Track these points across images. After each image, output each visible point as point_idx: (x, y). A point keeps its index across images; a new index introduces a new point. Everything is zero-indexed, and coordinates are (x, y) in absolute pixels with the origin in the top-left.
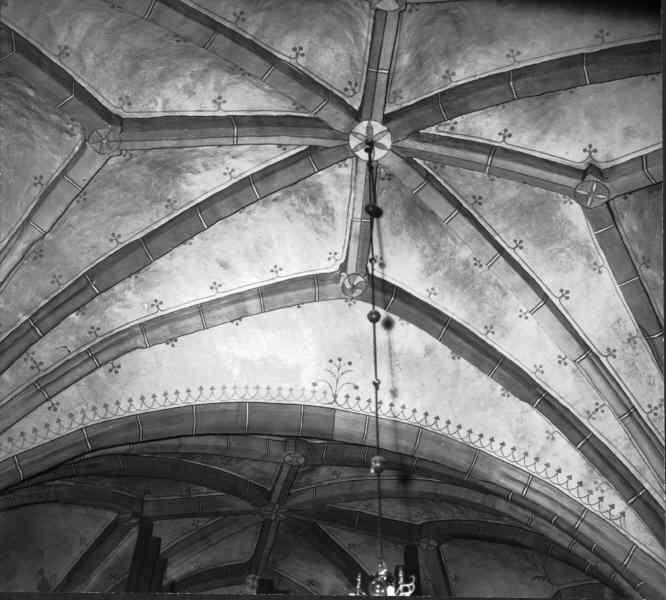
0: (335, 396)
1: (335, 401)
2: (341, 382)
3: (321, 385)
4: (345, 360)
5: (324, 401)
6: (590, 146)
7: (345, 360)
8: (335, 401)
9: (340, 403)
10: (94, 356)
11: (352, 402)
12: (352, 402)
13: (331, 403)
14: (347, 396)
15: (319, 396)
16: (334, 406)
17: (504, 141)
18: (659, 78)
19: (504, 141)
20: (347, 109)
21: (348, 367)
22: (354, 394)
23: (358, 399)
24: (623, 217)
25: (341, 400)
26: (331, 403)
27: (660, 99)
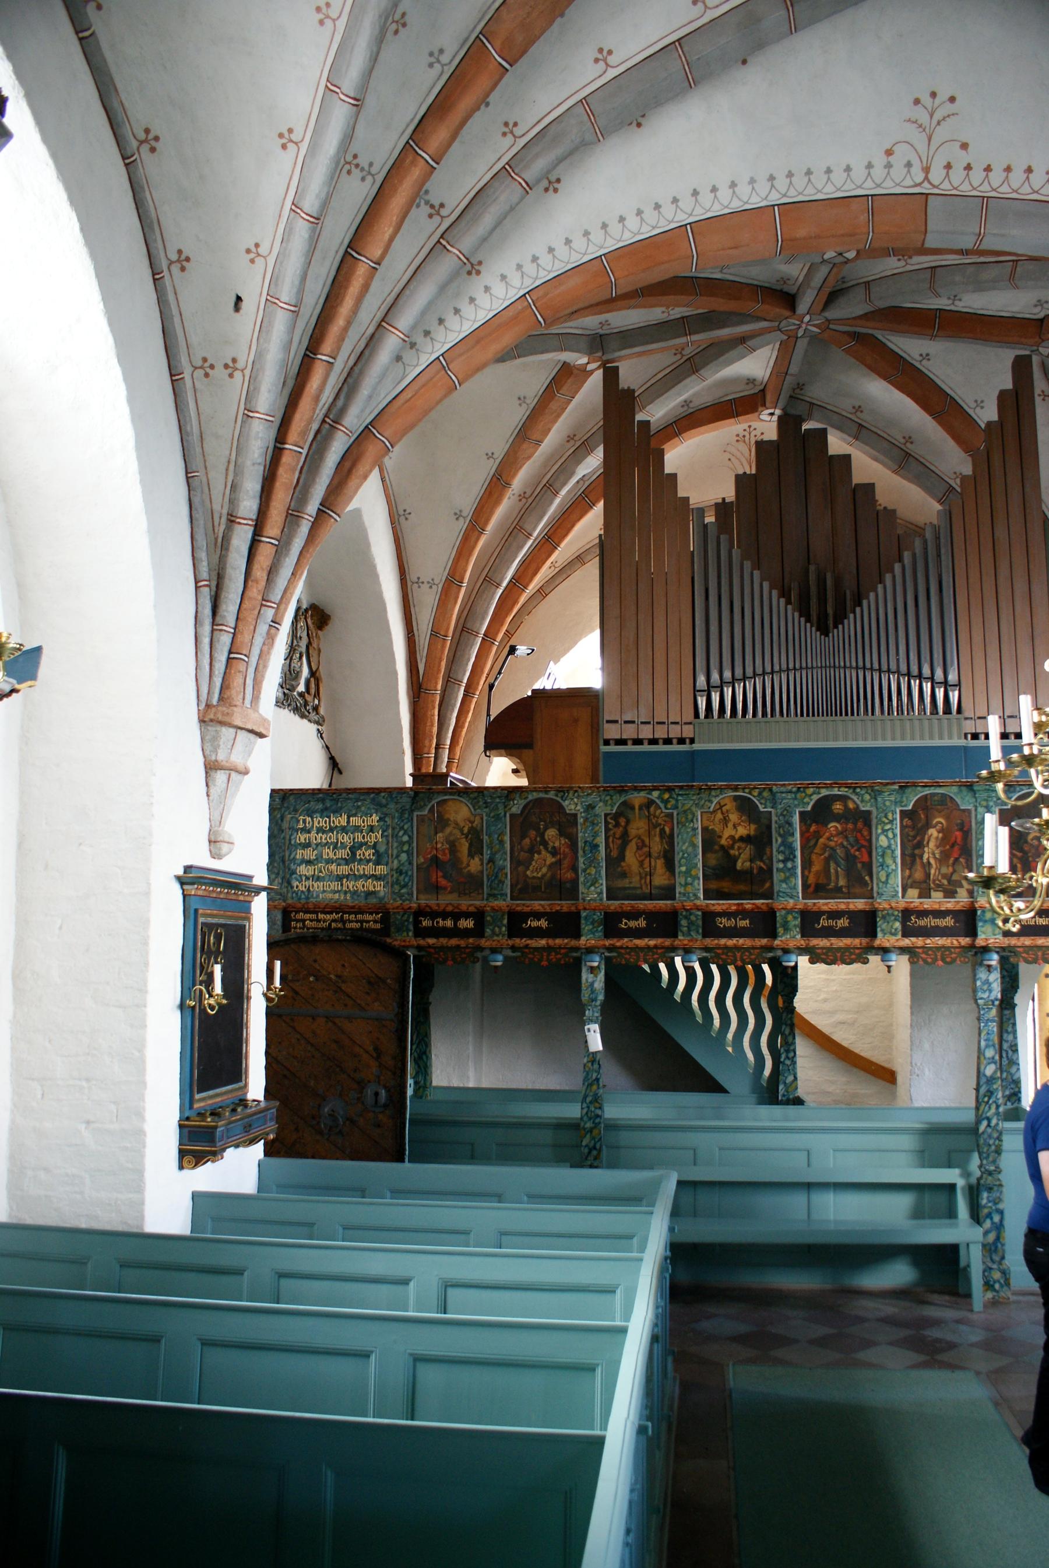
0: (927, 170)
1: (926, 178)
2: (936, 141)
3: (903, 153)
4: (943, 96)
5: (908, 182)
6: (506, 124)
7: (943, 96)
8: (926, 178)
9: (936, 183)
10: (819, 788)
11: (957, 175)
12: (957, 175)
13: (919, 185)
14: (948, 166)
15: (898, 171)
16: (926, 189)
17: (689, 407)
18: (620, 387)
19: (689, 407)
20: (350, 317)
21: (949, 108)
22: (961, 159)
23: (968, 168)
24: (899, 260)
25: (937, 174)
26: (919, 185)
27: (1046, 589)
